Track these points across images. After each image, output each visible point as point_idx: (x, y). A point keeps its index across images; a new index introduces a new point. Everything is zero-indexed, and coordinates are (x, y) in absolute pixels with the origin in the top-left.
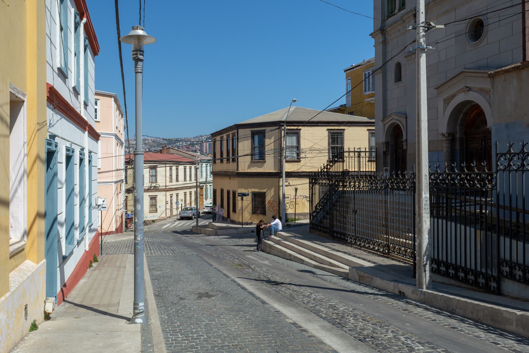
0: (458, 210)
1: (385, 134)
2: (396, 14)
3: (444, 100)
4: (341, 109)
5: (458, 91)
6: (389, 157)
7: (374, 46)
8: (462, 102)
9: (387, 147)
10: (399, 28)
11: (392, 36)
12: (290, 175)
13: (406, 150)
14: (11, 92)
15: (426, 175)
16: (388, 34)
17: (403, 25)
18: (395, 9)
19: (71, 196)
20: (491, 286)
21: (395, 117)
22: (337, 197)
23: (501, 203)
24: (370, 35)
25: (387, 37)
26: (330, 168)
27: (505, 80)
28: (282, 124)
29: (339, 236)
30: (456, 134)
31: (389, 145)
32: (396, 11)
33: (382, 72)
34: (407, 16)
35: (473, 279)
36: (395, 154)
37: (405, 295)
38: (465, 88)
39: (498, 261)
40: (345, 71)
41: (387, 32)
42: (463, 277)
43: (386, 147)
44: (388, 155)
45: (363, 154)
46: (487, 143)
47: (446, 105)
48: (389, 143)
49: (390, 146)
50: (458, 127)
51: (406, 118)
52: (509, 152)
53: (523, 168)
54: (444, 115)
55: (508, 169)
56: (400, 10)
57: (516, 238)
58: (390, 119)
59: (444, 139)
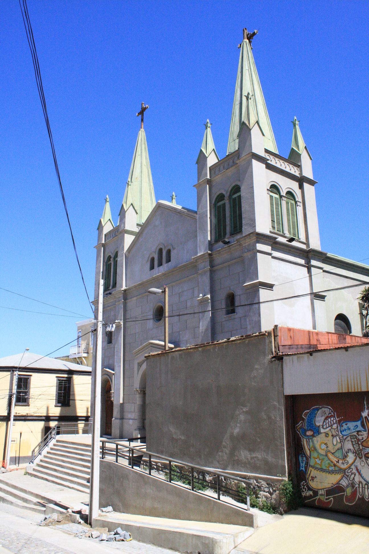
3: (138, 363)
12: (19, 418)
15: (98, 428)
18: (110, 286)
22: (291, 453)
28: (14, 369)
32: (110, 288)
37: (71, 522)
57: (191, 484)
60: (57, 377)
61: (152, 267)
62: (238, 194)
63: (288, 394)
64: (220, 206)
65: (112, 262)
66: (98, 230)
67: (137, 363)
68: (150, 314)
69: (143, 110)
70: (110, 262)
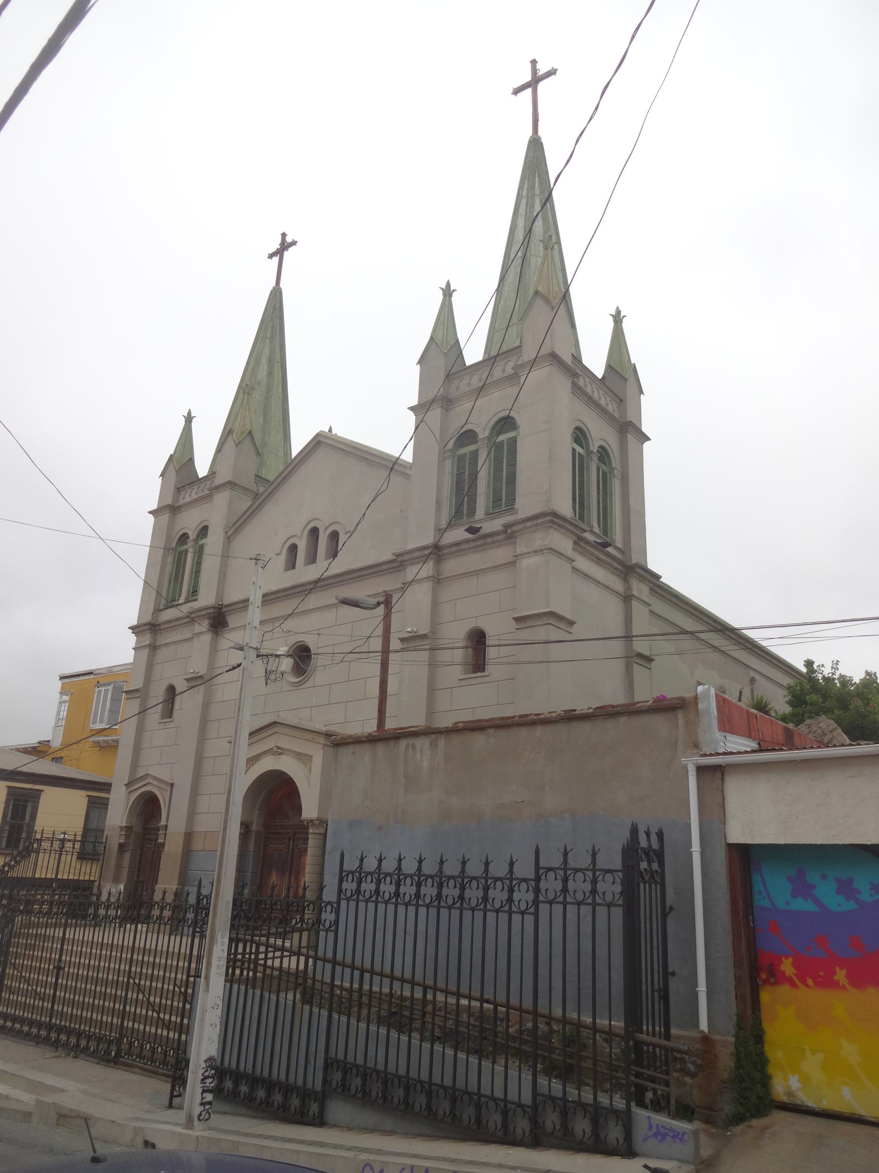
0: (261, 965)
1: (127, 812)
2: (181, 604)
4: (38, 749)
6: (127, 857)
7: (133, 649)
9: (127, 836)
13: (163, 845)
14: (465, 530)
20: (240, 1091)
23: (339, 957)
24: (129, 628)
26: (8, 872)
27: (353, 753)
29: (17, 1026)
30: (252, 824)
32: (181, 601)
35: (247, 1091)
39: (326, 1060)
40: (62, 678)
42: (264, 1097)
43: (125, 835)
44: (125, 851)
45: (68, 845)
46: (297, 846)
56: (187, 601)
60: (9, 787)
61: (291, 564)
62: (511, 434)
63: (735, 842)
64: (464, 455)
65: (190, 547)
66: (161, 477)
67: (718, 735)
68: (318, 661)
69: (285, 245)
70: (184, 548)
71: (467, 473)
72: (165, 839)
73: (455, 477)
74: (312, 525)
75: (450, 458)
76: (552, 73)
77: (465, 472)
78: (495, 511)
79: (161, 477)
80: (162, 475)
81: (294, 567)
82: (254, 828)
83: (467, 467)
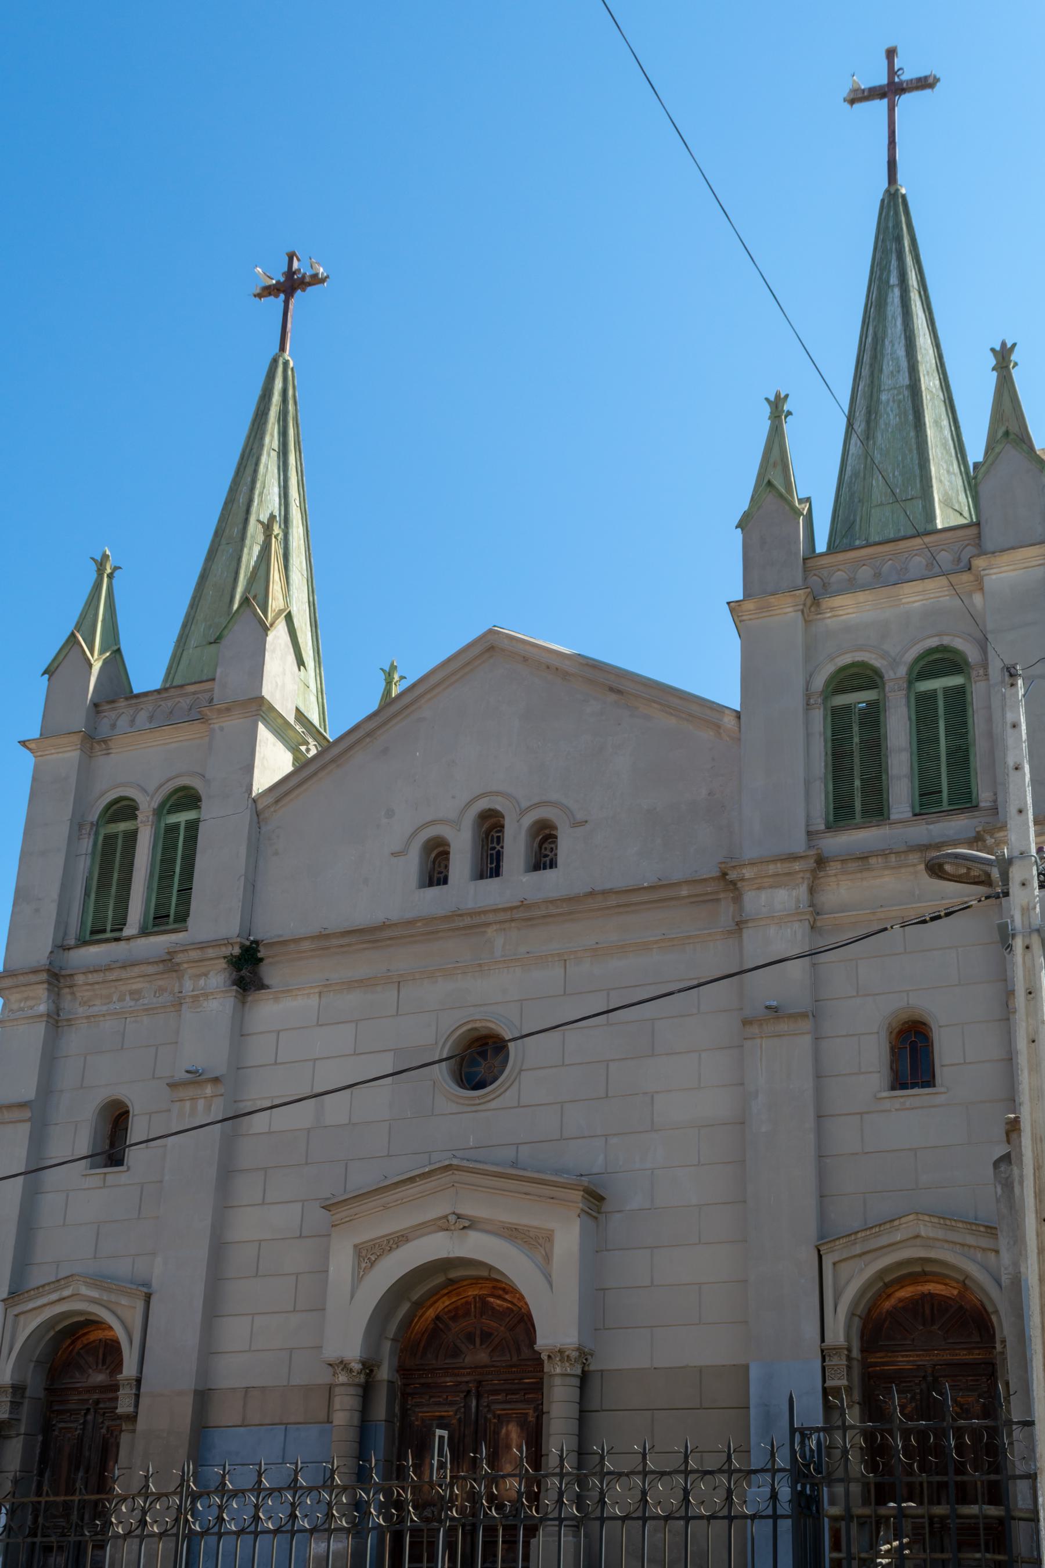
5: (420, 1224)
8: (70, 1310)
10: (135, 987)
11: (96, 1009)
13: (132, 1418)
16: (73, 993)
17: (160, 983)
19: (822, 557)
21: (84, 1290)
25: (67, 1003)
30: (379, 1367)
31: (23, 1397)
33: (30, 1120)
34: (194, 955)
36: (40, 1438)
38: (452, 1219)
41: (70, 987)
44: (9, 1437)
46: (488, 1406)
47: (363, 1265)
48: (25, 1389)
49: (26, 1401)
50: (387, 1346)
51: (148, 1298)
52: (143, 1491)
53: (293, 1525)
54: (352, 1297)
55: (216, 1529)
58: (54, 1297)
59: (342, 1378)
66: (46, 676)
71: (856, 740)
72: (137, 1405)
73: (829, 744)
74: (483, 804)
75: (819, 709)
76: (925, 83)
77: (852, 737)
78: (923, 811)
79: (46, 676)
80: (49, 672)
81: (496, 872)
82: (384, 1373)
83: (856, 729)
